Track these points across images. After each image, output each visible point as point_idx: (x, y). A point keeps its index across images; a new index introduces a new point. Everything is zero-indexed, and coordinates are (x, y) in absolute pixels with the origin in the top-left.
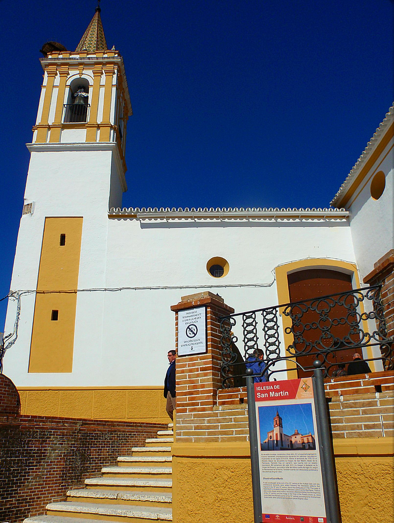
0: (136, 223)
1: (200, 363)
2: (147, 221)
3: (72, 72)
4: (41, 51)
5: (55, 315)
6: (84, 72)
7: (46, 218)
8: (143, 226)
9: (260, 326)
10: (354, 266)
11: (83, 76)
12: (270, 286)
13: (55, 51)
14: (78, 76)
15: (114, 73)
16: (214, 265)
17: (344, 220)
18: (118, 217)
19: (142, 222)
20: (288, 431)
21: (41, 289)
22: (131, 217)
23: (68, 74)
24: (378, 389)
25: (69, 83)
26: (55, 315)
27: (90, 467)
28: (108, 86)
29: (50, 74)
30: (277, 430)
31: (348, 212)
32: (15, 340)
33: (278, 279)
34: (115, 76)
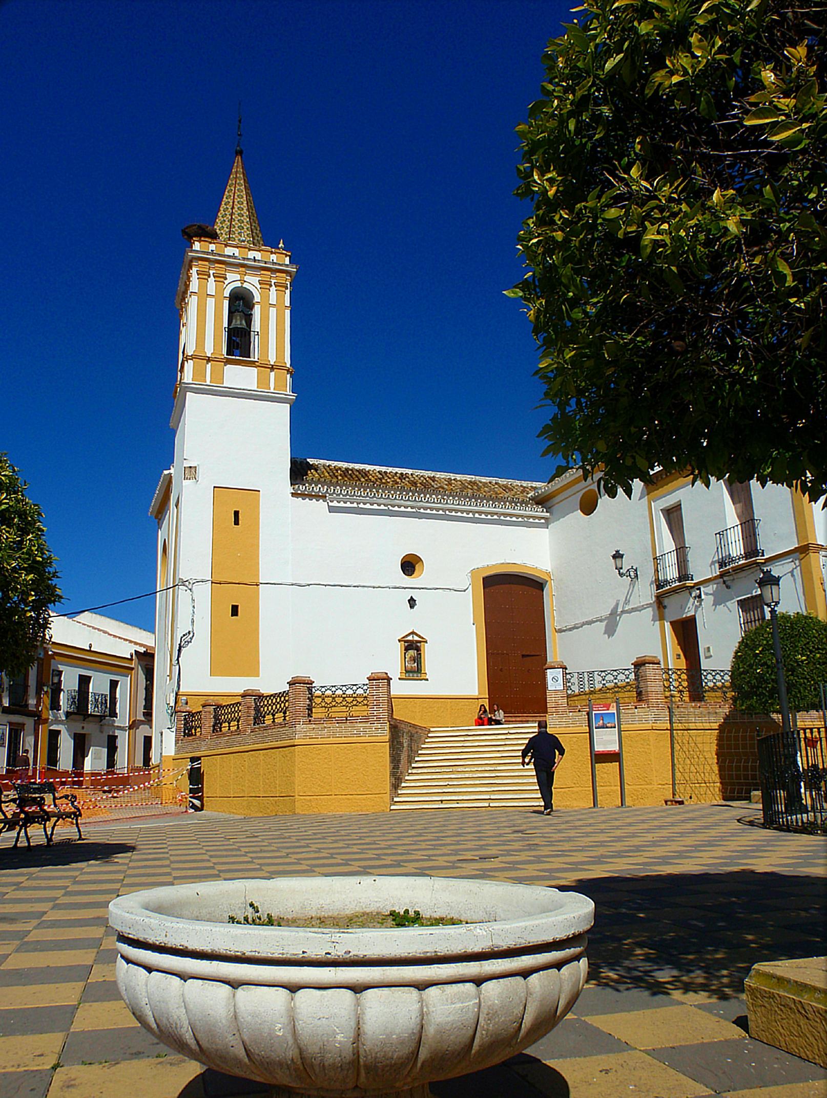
0: (322, 505)
1: (560, 694)
2: (335, 504)
3: (231, 276)
4: (184, 232)
5: (235, 611)
6: (246, 278)
7: (214, 487)
8: (332, 510)
9: (586, 679)
10: (548, 574)
11: (245, 285)
12: (465, 591)
13: (205, 237)
14: (238, 284)
15: (287, 288)
16: (409, 562)
17: (543, 521)
18: (303, 496)
19: (330, 504)
20: (605, 722)
21: (215, 579)
22: (318, 497)
23: (226, 279)
24: (636, 708)
25: (227, 293)
26: (235, 611)
27: (816, 696)
28: (278, 306)
29: (201, 274)
30: (601, 722)
31: (548, 514)
32: (191, 638)
33: (473, 584)
34: (288, 292)
